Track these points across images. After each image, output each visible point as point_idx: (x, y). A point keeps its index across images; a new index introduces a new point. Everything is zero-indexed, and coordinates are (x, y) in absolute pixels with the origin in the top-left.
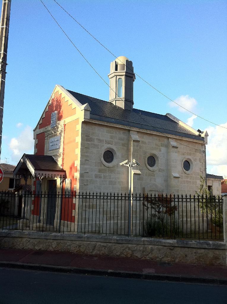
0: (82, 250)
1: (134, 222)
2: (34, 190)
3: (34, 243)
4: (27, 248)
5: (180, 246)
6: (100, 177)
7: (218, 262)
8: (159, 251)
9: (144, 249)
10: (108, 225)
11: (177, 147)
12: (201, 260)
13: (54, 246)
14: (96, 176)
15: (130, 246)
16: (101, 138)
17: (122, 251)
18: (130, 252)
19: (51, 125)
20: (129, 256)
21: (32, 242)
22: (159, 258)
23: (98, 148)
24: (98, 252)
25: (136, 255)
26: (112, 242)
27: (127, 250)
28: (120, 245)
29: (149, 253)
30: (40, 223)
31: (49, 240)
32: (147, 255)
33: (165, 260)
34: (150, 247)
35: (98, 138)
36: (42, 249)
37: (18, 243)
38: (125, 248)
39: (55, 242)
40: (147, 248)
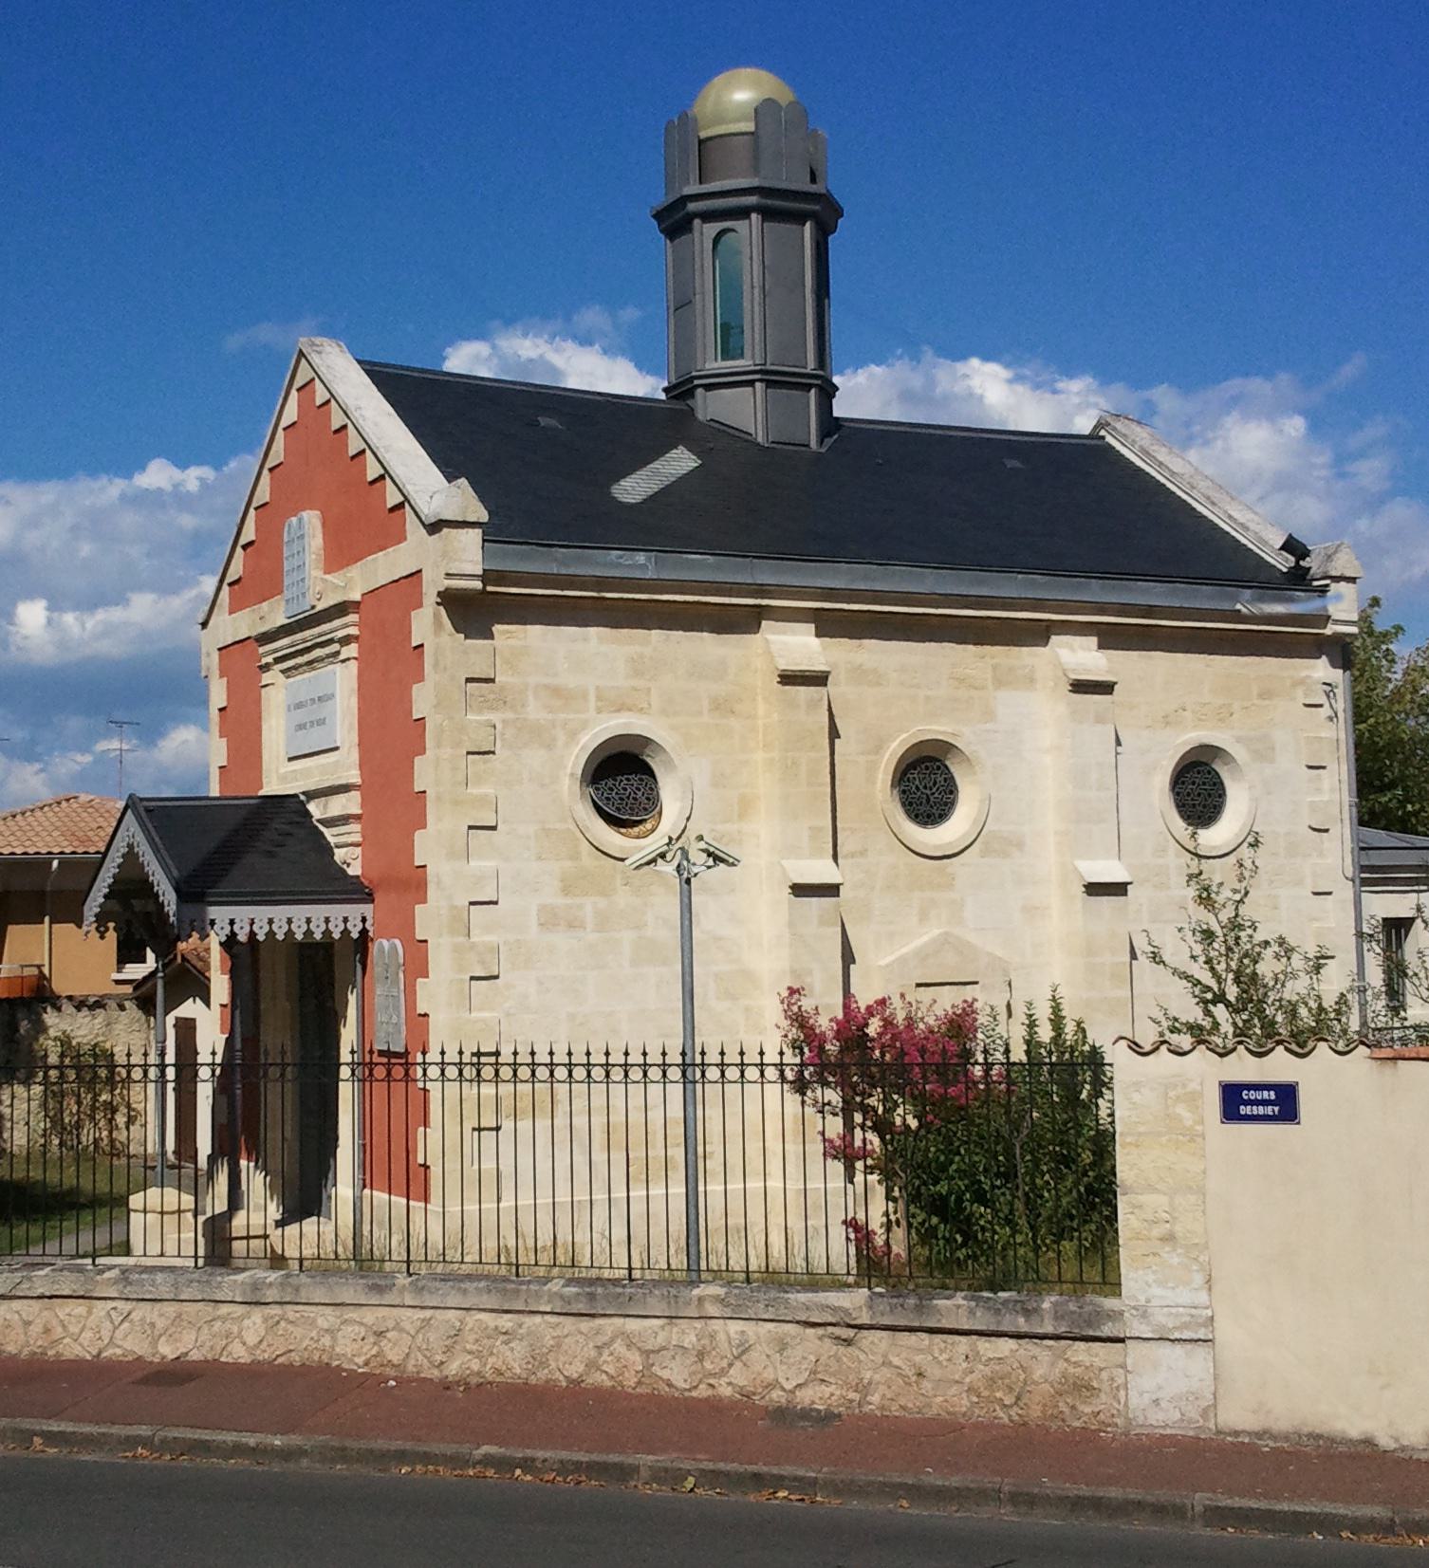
0: (394, 1355)
1: (657, 1191)
2: (1094, 640)
3: (153, 1325)
4: (119, 1351)
5: (887, 1321)
6: (573, 925)
7: (1088, 1410)
8: (781, 1351)
9: (705, 1341)
10: (638, 1208)
11: (1105, 688)
12: (998, 1395)
13: (251, 1339)
14: (550, 920)
15: (633, 1325)
16: (569, 680)
17: (593, 1353)
18: (636, 1359)
19: (287, 594)
20: (630, 1380)
21: (143, 1320)
22: (783, 1389)
23: (550, 747)
24: (475, 1365)
25: (665, 1374)
26: (542, 1309)
27: (618, 1346)
28: (585, 1325)
29: (730, 1365)
30: (426, 1200)
31: (224, 1309)
32: (723, 1372)
33: (814, 1397)
34: (734, 1327)
35: (546, 681)
36: (195, 1356)
37: (74, 1329)
38: (606, 1339)
39: (257, 1315)
40: (721, 1337)
